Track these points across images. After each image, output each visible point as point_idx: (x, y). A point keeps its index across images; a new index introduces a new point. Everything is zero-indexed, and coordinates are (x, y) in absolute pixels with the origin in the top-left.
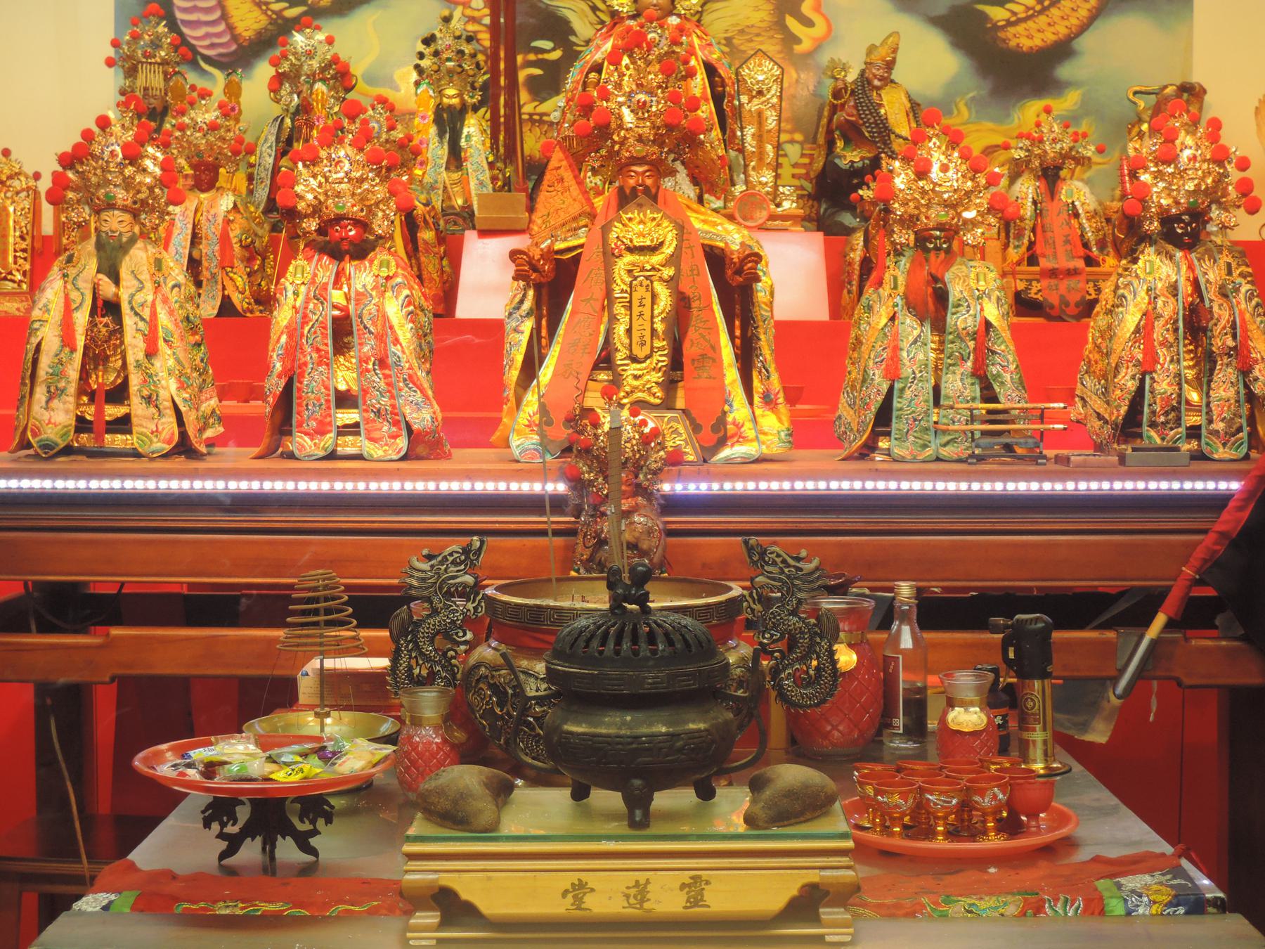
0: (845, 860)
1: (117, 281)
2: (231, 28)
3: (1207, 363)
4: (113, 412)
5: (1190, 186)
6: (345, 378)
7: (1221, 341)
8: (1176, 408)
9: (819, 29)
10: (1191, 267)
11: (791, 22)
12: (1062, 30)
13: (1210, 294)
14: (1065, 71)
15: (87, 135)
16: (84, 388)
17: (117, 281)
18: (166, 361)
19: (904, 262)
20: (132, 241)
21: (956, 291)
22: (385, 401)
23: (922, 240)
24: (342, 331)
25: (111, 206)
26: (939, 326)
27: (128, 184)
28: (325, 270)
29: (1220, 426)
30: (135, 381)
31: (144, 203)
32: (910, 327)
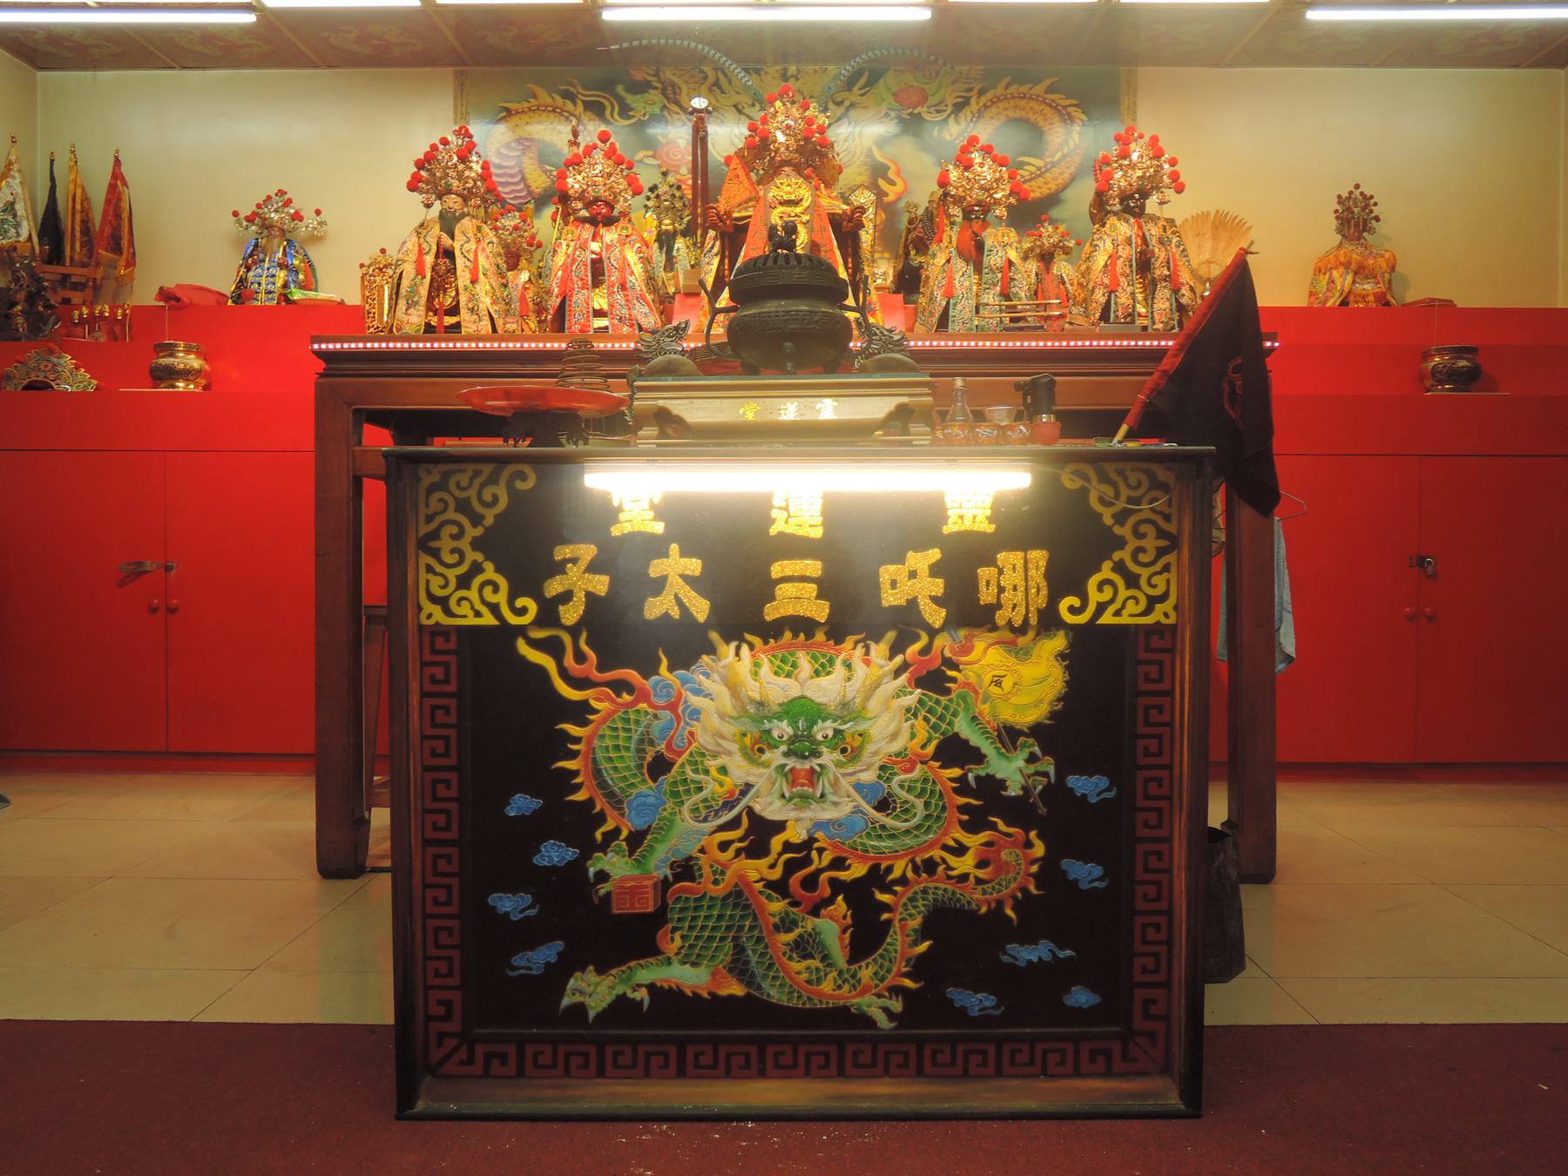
0: (926, 390)
1: (453, 238)
2: (527, 187)
3: (1150, 288)
4: (449, 320)
5: (1139, 173)
6: (600, 302)
7: (1160, 271)
8: (1131, 316)
9: (899, 187)
10: (1140, 227)
11: (882, 184)
12: (1053, 187)
13: (1153, 242)
14: (1055, 213)
15: (434, 147)
16: (430, 307)
17: (453, 238)
18: (483, 287)
19: (956, 228)
20: (463, 216)
21: (988, 244)
22: (625, 311)
23: (967, 213)
24: (598, 270)
25: (449, 192)
26: (978, 269)
27: (460, 176)
28: (587, 232)
29: (1160, 326)
30: (463, 299)
31: (470, 190)
32: (959, 265)
